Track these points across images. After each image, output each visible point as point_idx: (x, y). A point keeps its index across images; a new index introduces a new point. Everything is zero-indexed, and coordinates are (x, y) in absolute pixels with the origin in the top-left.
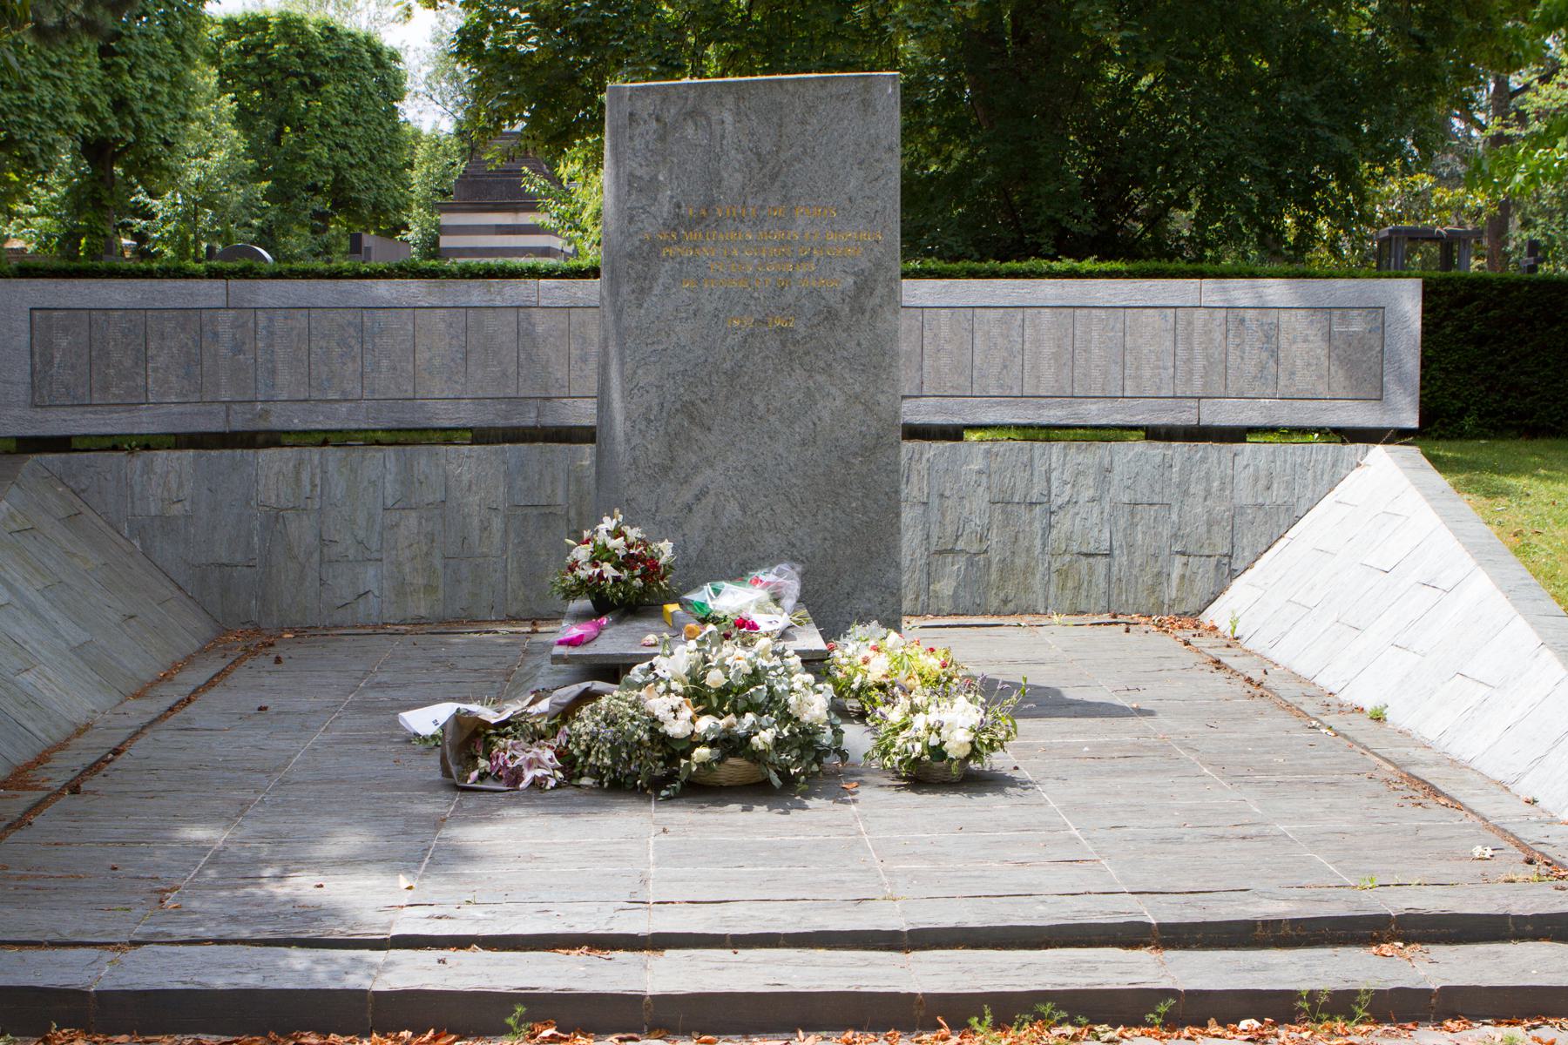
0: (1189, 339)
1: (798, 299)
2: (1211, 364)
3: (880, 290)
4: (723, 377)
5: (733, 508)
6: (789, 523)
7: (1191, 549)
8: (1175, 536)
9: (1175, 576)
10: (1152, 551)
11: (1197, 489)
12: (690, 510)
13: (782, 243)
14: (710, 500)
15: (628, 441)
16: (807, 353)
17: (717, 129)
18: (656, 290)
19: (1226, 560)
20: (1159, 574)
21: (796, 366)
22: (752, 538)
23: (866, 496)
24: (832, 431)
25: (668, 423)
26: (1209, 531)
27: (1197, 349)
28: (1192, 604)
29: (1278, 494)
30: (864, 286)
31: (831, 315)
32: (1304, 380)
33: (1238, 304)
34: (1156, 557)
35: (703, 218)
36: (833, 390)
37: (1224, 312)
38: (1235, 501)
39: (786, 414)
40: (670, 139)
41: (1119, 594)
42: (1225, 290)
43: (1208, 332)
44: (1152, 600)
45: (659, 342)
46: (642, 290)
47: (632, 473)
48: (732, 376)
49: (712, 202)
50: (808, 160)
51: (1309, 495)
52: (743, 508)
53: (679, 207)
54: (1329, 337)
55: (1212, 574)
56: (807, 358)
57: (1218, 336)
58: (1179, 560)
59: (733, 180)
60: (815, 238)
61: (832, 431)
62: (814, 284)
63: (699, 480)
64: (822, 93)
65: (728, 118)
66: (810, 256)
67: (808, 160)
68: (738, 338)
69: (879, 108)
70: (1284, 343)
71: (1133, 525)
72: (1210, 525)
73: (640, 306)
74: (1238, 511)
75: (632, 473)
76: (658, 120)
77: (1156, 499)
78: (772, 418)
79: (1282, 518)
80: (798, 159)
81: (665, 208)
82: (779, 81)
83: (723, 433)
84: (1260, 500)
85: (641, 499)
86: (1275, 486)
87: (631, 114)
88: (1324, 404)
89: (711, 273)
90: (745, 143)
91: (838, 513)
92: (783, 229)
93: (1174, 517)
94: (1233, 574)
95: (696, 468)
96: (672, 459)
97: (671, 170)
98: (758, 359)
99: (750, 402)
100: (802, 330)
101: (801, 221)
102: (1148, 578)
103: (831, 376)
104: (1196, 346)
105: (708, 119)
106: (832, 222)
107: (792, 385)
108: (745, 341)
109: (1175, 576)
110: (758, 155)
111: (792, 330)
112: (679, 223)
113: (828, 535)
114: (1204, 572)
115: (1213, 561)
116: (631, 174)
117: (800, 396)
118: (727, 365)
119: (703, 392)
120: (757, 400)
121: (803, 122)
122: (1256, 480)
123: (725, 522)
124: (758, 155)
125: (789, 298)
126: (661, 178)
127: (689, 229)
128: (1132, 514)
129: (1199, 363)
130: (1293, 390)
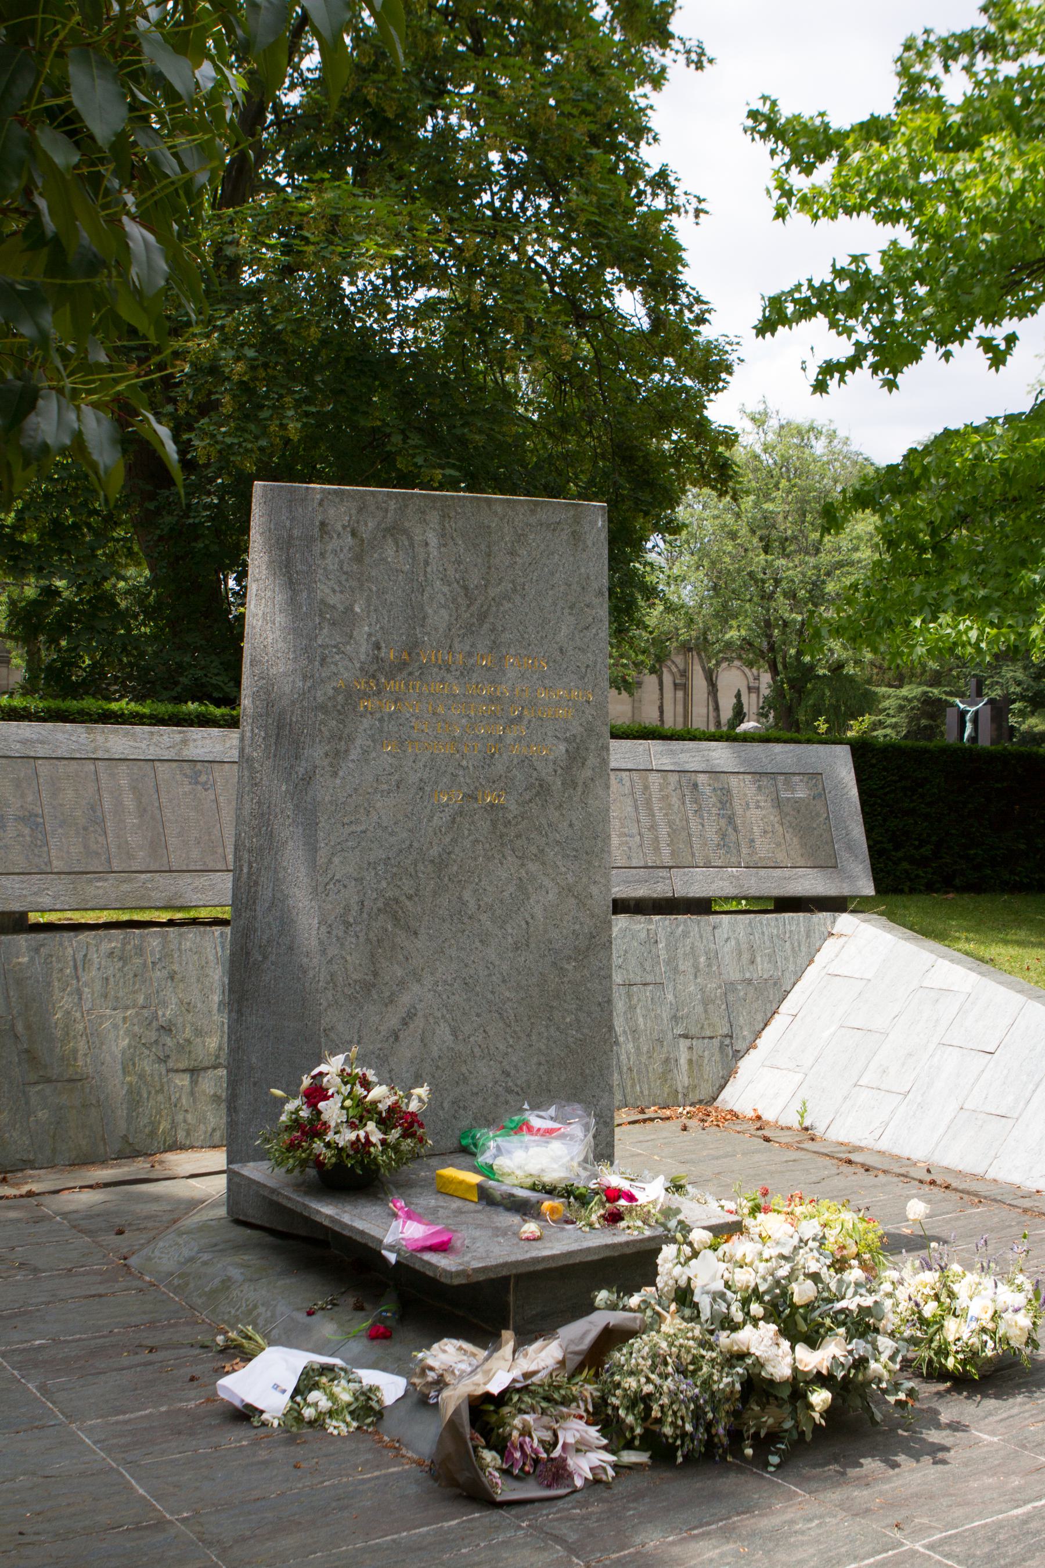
0: (648, 802)
1: (509, 770)
2: (674, 831)
3: (592, 761)
4: (430, 868)
5: (443, 1032)
6: (502, 1047)
7: (693, 1031)
8: (675, 1018)
9: (683, 1061)
10: (655, 1036)
11: (685, 965)
12: (397, 1038)
13: (493, 700)
14: (419, 1022)
15: (324, 952)
16: (518, 836)
17: (420, 550)
18: (354, 754)
19: (727, 1041)
20: (667, 1060)
21: (508, 852)
22: (464, 1069)
23: (580, 1009)
24: (546, 931)
25: (369, 927)
26: (706, 1011)
27: (659, 815)
28: (704, 1092)
29: (763, 968)
30: (576, 756)
31: (543, 789)
32: (764, 848)
33: (688, 767)
34: (661, 1041)
35: (405, 664)
36: (546, 882)
37: (676, 776)
38: (725, 977)
39: (498, 912)
40: (367, 560)
41: (633, 1086)
42: (672, 752)
43: (665, 798)
44: (666, 1090)
45: (357, 822)
46: (337, 753)
47: (329, 994)
48: (440, 864)
49: (416, 644)
50: (518, 599)
51: (792, 968)
52: (454, 1033)
53: (379, 648)
54: (778, 803)
55: (717, 1057)
56: (519, 843)
57: (675, 800)
58: (684, 1044)
59: (439, 618)
60: (526, 695)
61: (546, 931)
62: (525, 751)
63: (405, 999)
64: (533, 520)
65: (433, 540)
66: (520, 717)
67: (518, 599)
68: (446, 817)
69: (589, 543)
70: (739, 810)
71: (632, 1008)
72: (706, 1002)
73: (335, 774)
74: (730, 987)
75: (329, 994)
76: (354, 534)
77: (649, 978)
78: (484, 917)
79: (770, 995)
80: (506, 597)
81: (363, 650)
82: (487, 500)
83: (431, 938)
84: (748, 975)
85: (340, 1027)
86: (759, 959)
87: (323, 524)
88: (787, 872)
89: (415, 734)
90: (451, 572)
91: (552, 1030)
92: (492, 682)
93: (670, 997)
94: (738, 1055)
95: (402, 983)
96: (375, 974)
97: (368, 600)
98: (467, 843)
99: (460, 898)
100: (513, 807)
101: (511, 674)
102: (657, 1066)
103: (544, 864)
104: (657, 813)
105: (410, 539)
106: (543, 677)
107: (505, 875)
108: (453, 821)
109: (683, 1061)
110: (466, 588)
111: (503, 808)
112: (378, 669)
113: (543, 1059)
114: (710, 1052)
115: (716, 1042)
116: (322, 601)
117: (512, 889)
118: (434, 852)
119: (408, 885)
120: (467, 895)
121: (512, 553)
122: (740, 954)
123: (435, 1054)
124: (466, 588)
125: (500, 768)
126: (357, 609)
127: (390, 677)
128: (629, 996)
129: (663, 831)
130: (756, 858)
